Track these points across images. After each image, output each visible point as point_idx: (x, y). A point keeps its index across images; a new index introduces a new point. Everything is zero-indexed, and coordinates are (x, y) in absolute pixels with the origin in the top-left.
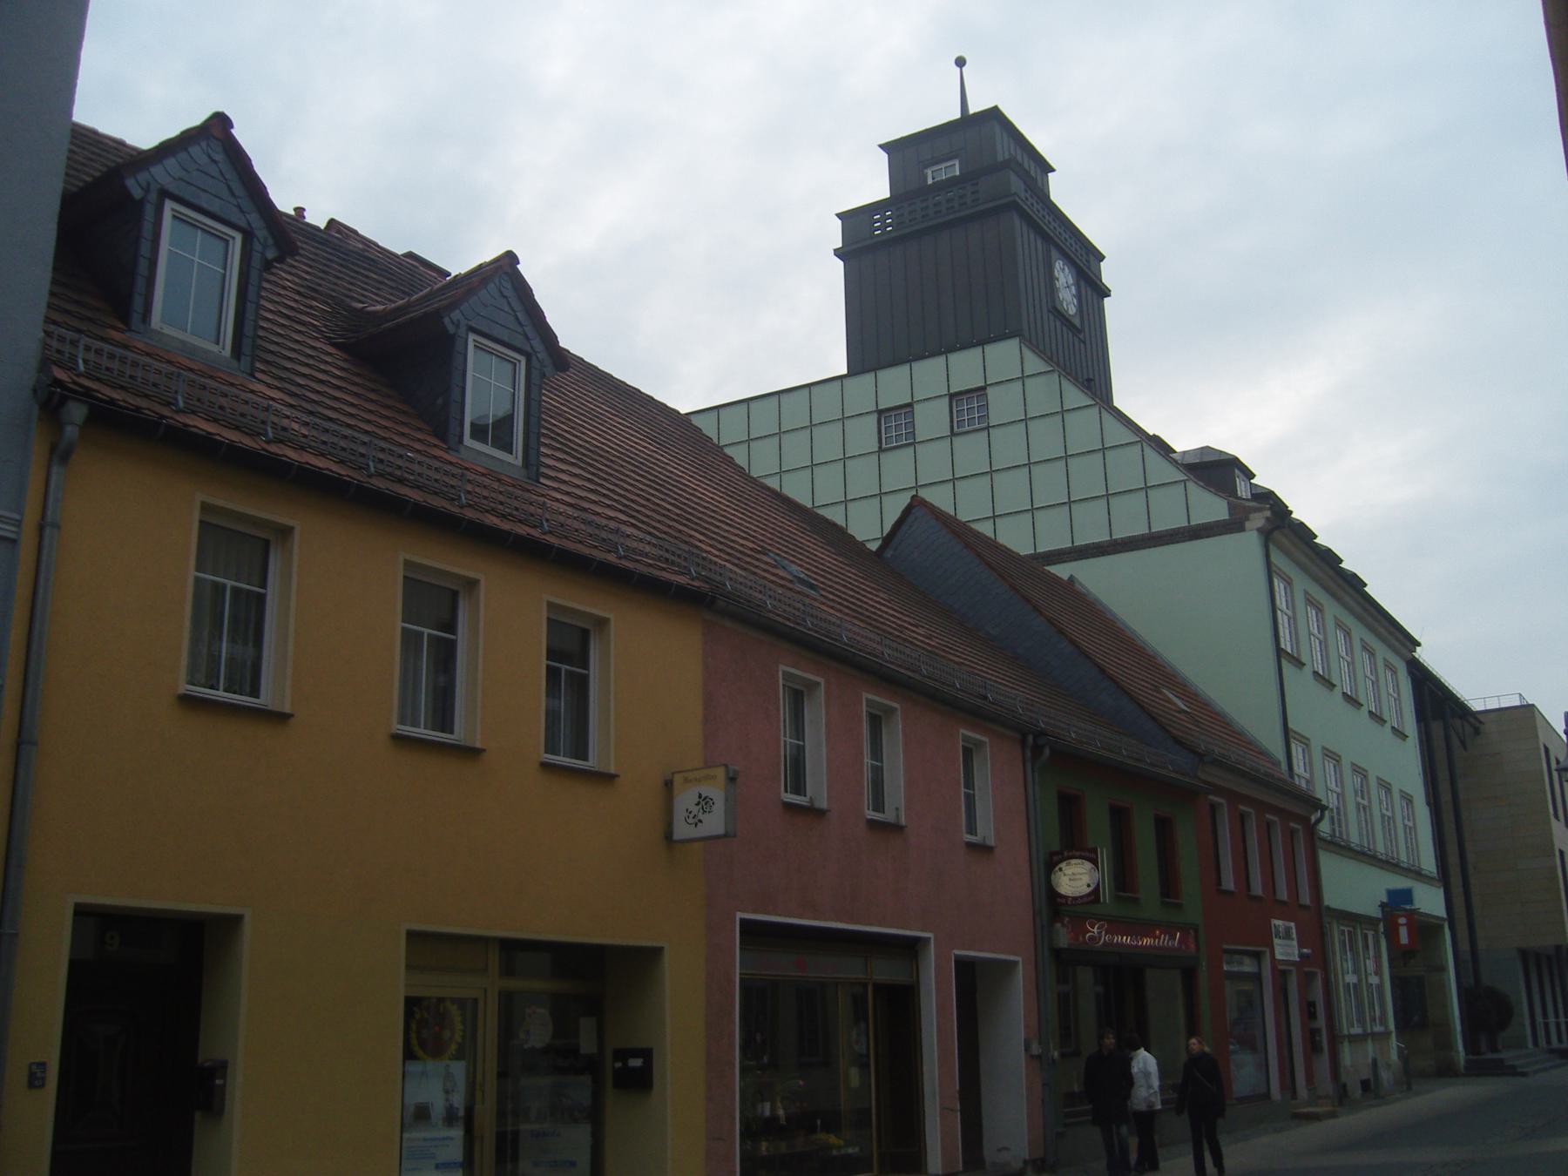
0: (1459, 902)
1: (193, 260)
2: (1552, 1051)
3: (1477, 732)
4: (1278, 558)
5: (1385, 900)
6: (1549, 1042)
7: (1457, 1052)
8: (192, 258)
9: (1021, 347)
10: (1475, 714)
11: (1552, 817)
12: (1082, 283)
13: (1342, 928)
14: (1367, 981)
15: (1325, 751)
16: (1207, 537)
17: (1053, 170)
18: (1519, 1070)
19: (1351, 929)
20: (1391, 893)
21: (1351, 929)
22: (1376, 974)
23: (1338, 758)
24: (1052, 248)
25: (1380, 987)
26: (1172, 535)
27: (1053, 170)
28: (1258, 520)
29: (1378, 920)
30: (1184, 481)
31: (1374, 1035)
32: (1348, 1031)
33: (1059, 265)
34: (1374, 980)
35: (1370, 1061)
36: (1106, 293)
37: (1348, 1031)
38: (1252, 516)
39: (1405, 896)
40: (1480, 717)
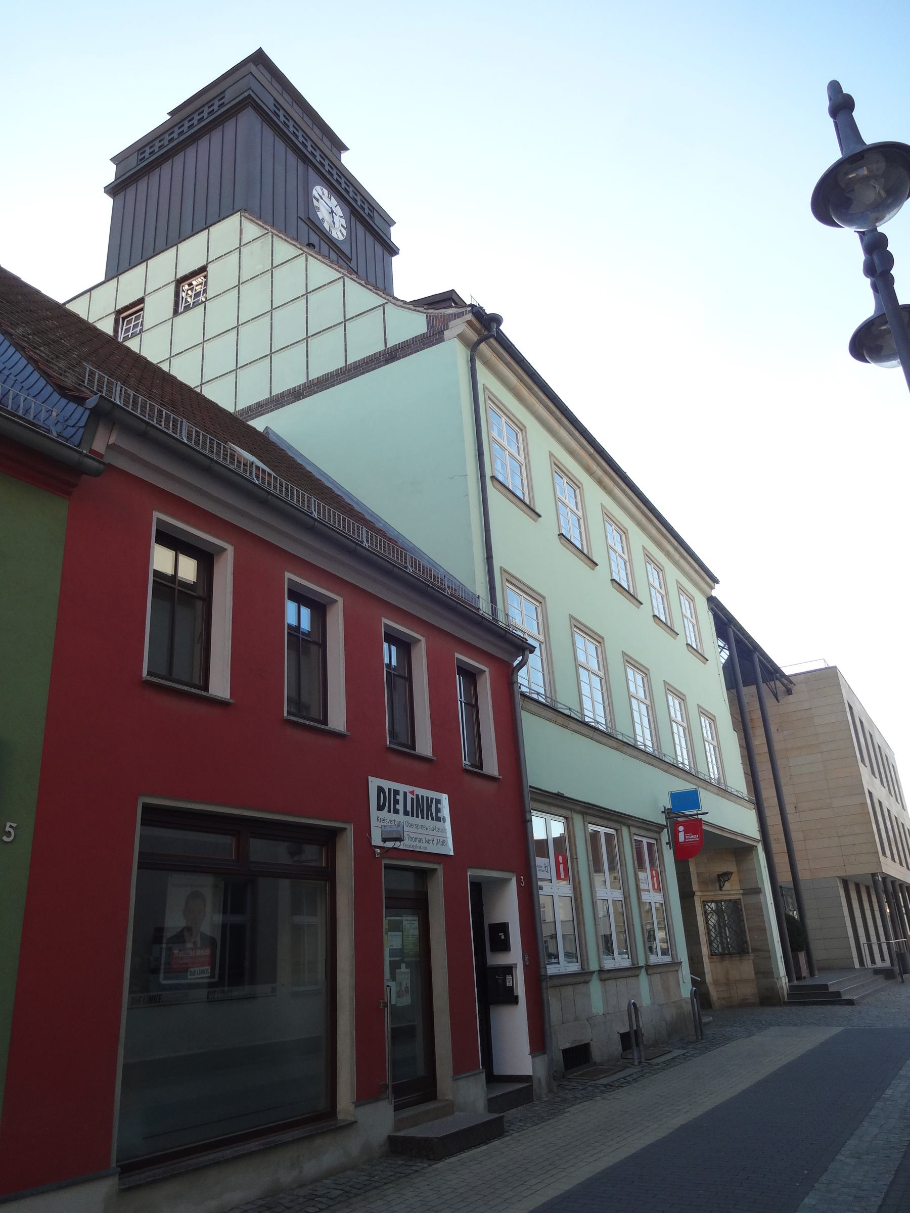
0: (773, 820)
1: (175, 588)
2: (877, 972)
3: (789, 692)
4: (484, 376)
5: (669, 806)
6: (873, 961)
7: (779, 978)
8: (172, 586)
9: (241, 220)
10: (787, 678)
11: (860, 764)
12: (353, 219)
13: (592, 827)
14: (639, 898)
15: (574, 622)
16: (403, 357)
17: (346, 149)
18: (846, 997)
19: (612, 831)
20: (674, 796)
21: (612, 831)
22: (658, 890)
23: (601, 640)
24: (310, 169)
25: (666, 904)
26: (367, 363)
27: (346, 149)
28: (459, 326)
29: (661, 827)
30: (383, 305)
31: (649, 968)
32: (647, 959)
33: (318, 190)
34: (653, 898)
35: (625, 1007)
36: (393, 251)
37: (647, 959)
38: (451, 324)
39: (689, 799)
40: (792, 679)
